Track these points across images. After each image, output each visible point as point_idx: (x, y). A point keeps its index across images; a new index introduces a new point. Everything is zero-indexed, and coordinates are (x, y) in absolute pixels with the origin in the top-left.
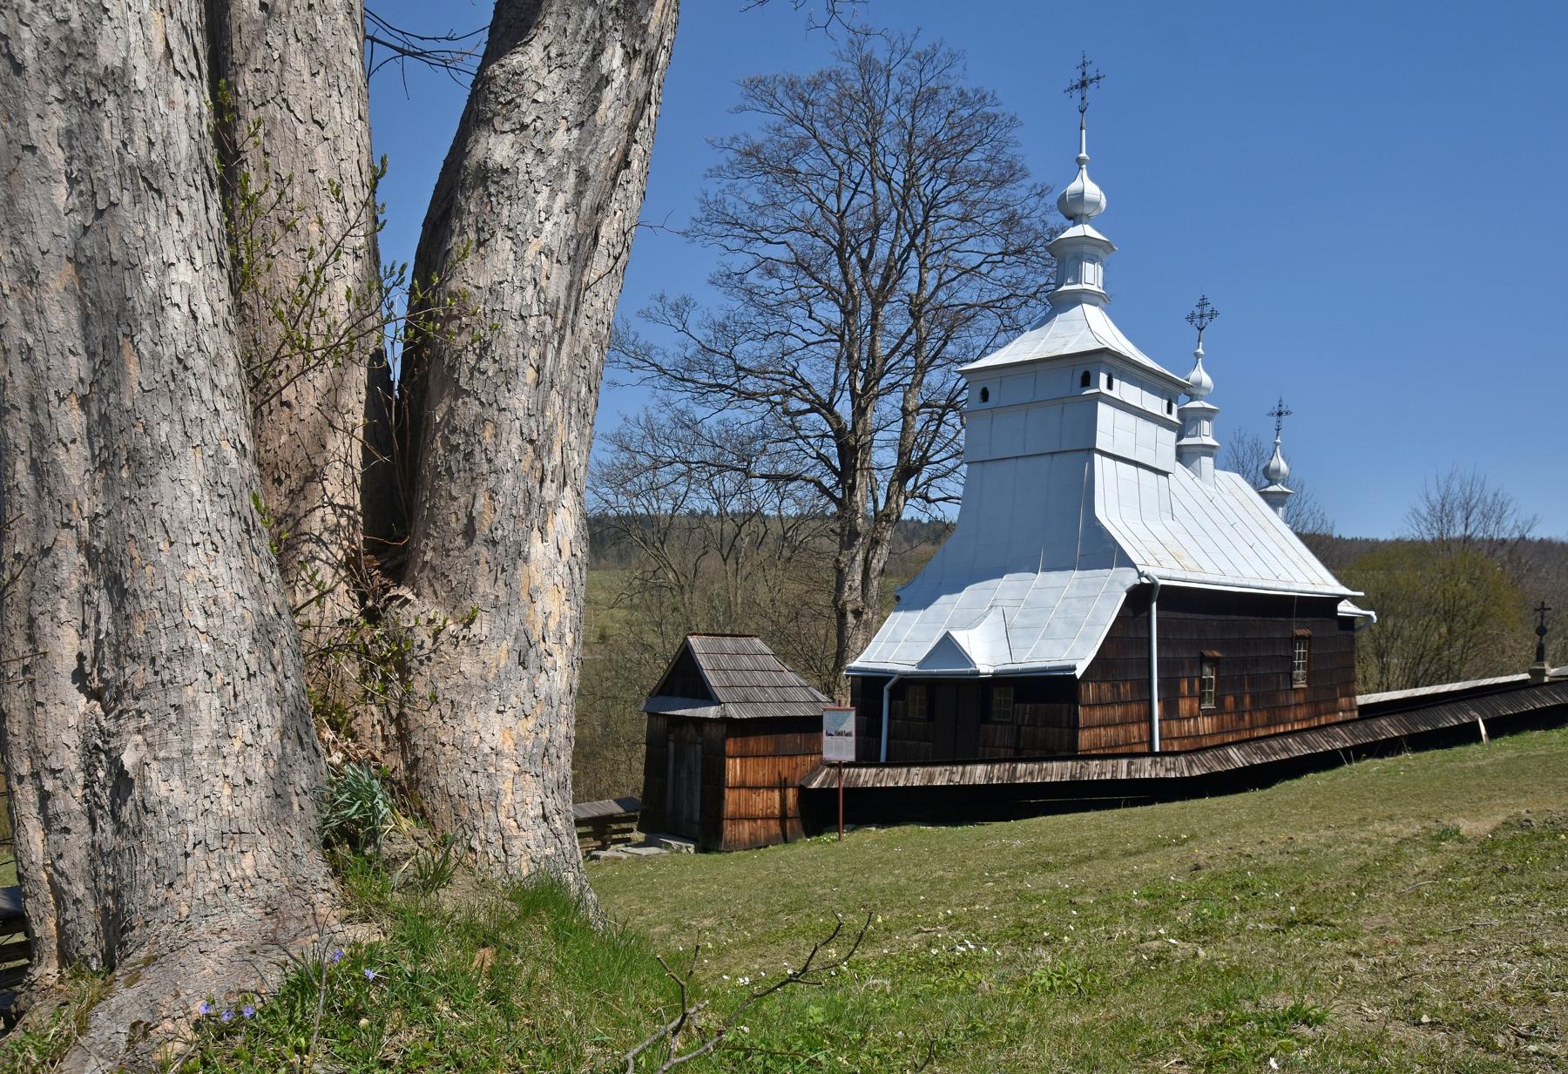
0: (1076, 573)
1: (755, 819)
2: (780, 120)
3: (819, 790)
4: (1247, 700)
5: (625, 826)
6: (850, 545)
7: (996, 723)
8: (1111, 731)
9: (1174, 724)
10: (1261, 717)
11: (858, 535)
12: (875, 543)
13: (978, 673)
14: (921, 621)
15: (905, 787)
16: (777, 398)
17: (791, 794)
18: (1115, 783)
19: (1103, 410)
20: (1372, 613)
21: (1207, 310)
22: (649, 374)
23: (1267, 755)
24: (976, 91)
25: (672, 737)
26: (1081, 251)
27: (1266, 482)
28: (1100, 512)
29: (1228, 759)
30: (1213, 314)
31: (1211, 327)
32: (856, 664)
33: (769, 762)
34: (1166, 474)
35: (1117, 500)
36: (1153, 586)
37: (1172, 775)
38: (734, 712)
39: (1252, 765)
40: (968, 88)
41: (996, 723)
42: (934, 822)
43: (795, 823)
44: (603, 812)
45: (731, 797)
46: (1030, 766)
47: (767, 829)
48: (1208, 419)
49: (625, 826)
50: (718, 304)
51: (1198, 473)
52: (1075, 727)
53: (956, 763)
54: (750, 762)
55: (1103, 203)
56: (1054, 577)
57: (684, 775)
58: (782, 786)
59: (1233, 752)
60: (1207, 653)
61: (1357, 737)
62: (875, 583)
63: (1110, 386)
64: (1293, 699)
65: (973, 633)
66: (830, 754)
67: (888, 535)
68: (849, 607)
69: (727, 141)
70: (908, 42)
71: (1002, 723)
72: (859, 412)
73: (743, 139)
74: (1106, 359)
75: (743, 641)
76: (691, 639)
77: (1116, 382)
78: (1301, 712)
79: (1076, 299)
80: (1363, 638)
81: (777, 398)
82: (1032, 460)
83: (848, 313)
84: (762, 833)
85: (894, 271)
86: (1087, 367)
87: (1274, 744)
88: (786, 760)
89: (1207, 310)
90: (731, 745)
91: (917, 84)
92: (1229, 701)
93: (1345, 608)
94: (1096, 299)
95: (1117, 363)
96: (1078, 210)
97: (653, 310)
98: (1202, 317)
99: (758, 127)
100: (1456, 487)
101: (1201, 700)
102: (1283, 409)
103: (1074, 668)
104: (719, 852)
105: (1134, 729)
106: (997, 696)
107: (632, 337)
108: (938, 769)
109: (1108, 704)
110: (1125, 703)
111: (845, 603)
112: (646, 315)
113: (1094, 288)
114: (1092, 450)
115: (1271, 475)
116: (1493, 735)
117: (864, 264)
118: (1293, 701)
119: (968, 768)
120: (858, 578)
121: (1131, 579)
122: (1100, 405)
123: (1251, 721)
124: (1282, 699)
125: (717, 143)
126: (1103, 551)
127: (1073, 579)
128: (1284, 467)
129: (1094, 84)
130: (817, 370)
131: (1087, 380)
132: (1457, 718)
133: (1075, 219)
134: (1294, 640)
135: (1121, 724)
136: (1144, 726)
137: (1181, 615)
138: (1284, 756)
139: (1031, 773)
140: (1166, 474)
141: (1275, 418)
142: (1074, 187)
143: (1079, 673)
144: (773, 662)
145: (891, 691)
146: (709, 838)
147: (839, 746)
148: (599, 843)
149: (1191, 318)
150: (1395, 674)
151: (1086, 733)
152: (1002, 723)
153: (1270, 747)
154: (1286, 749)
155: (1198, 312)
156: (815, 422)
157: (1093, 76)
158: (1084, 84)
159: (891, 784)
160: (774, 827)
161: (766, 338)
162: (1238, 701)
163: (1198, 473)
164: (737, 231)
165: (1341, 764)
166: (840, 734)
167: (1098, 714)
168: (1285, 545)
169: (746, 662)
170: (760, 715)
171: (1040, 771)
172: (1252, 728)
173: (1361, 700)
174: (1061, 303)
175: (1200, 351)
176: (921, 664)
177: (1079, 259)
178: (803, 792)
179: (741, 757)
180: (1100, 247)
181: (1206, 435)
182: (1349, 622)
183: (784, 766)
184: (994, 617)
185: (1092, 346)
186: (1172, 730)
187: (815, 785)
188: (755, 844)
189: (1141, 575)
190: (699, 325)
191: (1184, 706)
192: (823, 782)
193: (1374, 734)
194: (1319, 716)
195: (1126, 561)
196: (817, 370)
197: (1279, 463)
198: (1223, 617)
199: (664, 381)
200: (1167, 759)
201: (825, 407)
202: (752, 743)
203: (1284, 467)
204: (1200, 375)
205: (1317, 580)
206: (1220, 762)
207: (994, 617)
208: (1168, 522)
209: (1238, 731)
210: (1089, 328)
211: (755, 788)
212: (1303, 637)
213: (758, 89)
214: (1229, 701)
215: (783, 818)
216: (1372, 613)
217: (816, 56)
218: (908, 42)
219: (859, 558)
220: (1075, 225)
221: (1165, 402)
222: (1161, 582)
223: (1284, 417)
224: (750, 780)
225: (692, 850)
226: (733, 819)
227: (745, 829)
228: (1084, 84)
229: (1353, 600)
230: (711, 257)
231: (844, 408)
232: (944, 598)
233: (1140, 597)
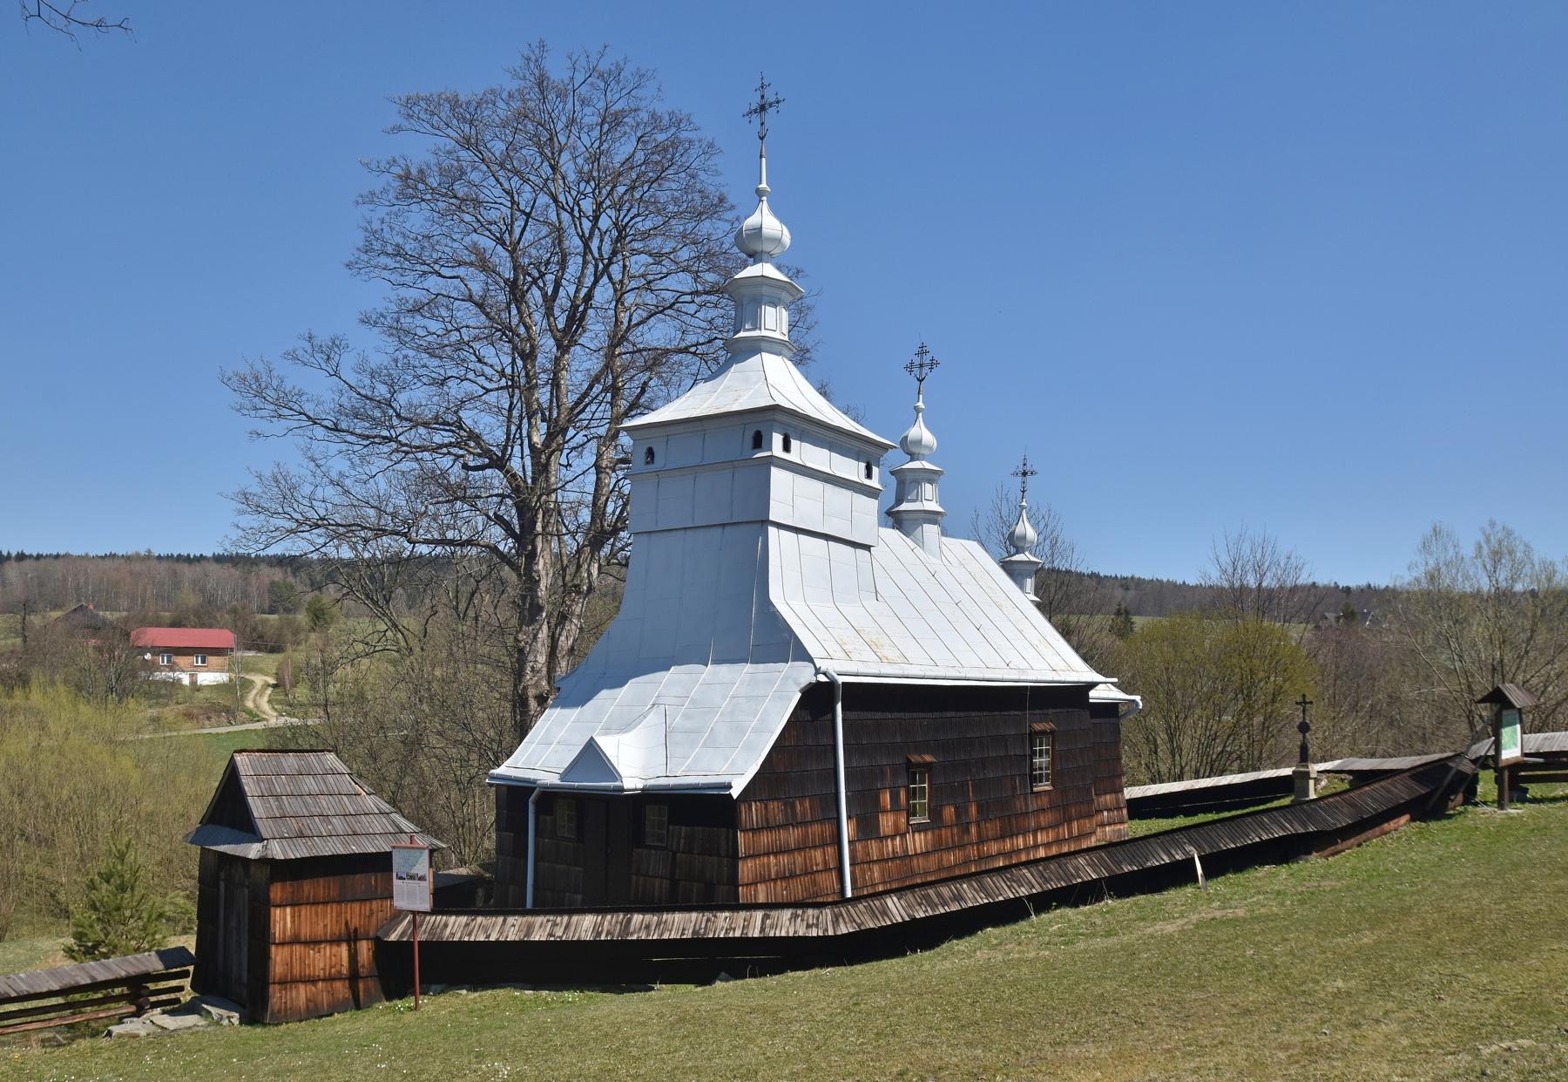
0: (748, 667)
1: (313, 981)
3: (398, 943)
4: (973, 809)
5: (174, 983)
6: (532, 621)
7: (651, 847)
8: (784, 859)
9: (874, 846)
10: (992, 828)
11: (541, 609)
12: (563, 618)
13: (622, 789)
14: (577, 720)
15: (497, 942)
17: (365, 948)
18: (745, 943)
19: (777, 476)
20: (1138, 698)
22: (296, 424)
23: (934, 906)
24: (671, 114)
25: (222, 875)
26: (763, 293)
27: (1013, 550)
28: (775, 595)
29: (885, 912)
30: (933, 364)
31: (931, 377)
32: (502, 770)
33: (332, 910)
34: (867, 548)
35: (796, 582)
36: (832, 684)
37: (814, 933)
38: (277, 851)
39: (914, 920)
40: (661, 109)
41: (651, 847)
42: (536, 985)
43: (371, 983)
44: (142, 969)
45: (279, 956)
46: (648, 917)
47: (332, 993)
48: (931, 482)
49: (174, 983)
50: (376, 348)
51: (921, 543)
52: (734, 857)
53: (561, 912)
54: (305, 911)
55: (787, 238)
56: (724, 669)
57: (233, 924)
58: (352, 938)
59: (892, 903)
60: (915, 758)
61: (1047, 881)
62: (564, 664)
63: (787, 448)
64: (1033, 805)
65: (628, 738)
66: (400, 902)
67: (577, 609)
68: (532, 692)
69: (383, 165)
70: (593, 59)
71: (656, 848)
72: (541, 469)
73: (401, 162)
74: (778, 416)
75: (312, 757)
76: (238, 758)
77: (794, 443)
78: (1044, 819)
79: (755, 347)
80: (1126, 726)
82: (700, 533)
84: (325, 998)
86: (761, 425)
87: (945, 891)
88: (356, 906)
90: (277, 892)
91: (601, 105)
92: (949, 812)
94: (778, 348)
95: (795, 422)
96: (758, 248)
97: (300, 352)
98: (922, 366)
99: (423, 149)
100: (1246, 550)
101: (911, 812)
102: (1028, 469)
103: (729, 787)
104: (264, 1025)
105: (818, 855)
106: (653, 815)
108: (540, 919)
109: (779, 827)
110: (803, 824)
111: (525, 688)
113: (777, 335)
114: (766, 522)
115: (1015, 543)
116: (1208, 875)
117: (549, 301)
118: (1033, 806)
119: (575, 918)
120: (542, 659)
121: (806, 675)
122: (773, 470)
123: (979, 833)
124: (1019, 805)
126: (779, 643)
127: (742, 674)
128: (1031, 534)
131: (759, 441)
132: (1170, 854)
133: (755, 256)
134: (1033, 735)
135: (799, 849)
136: (830, 850)
137: (878, 715)
138: (955, 907)
139: (648, 927)
140: (867, 548)
141: (1020, 478)
142: (752, 221)
143: (735, 793)
144: (346, 783)
145: (537, 803)
146: (255, 1011)
147: (412, 893)
148: (133, 1009)
149: (910, 368)
150: (1189, 755)
151: (750, 863)
152: (656, 848)
153: (939, 895)
154: (958, 898)
155: (917, 361)
157: (772, 99)
158: (763, 108)
159: (482, 938)
160: (341, 989)
162: (961, 812)
163: (921, 543)
165: (1027, 915)
166: (412, 877)
167: (765, 839)
168: (1024, 625)
169: (310, 784)
170: (314, 853)
171: (658, 924)
172: (981, 841)
173: (1132, 792)
174: (741, 351)
175: (920, 404)
176: (563, 776)
177: (758, 302)
178: (381, 947)
179: (292, 905)
180: (783, 289)
181: (929, 499)
182: (1110, 709)
183: (355, 914)
184: (654, 718)
185: (772, 403)
186: (878, 850)
187: (393, 937)
188: (315, 1012)
189: (818, 671)
191: (886, 822)
192: (402, 935)
193: (1069, 876)
194: (1070, 821)
195: (803, 655)
197: (1026, 529)
198: (937, 715)
199: (319, 432)
200: (810, 912)
202: (307, 888)
203: (1031, 534)
204: (921, 432)
206: (874, 916)
207: (654, 718)
208: (871, 603)
209: (962, 846)
210: (774, 380)
211: (314, 942)
212: (1043, 733)
214: (949, 812)
215: (354, 977)
216: (1138, 698)
217: (486, 71)
218: (593, 59)
219: (544, 633)
220: (755, 263)
221: (863, 465)
222: (841, 680)
223: (1028, 477)
224: (305, 932)
225: (236, 1021)
226: (283, 983)
227: (302, 994)
228: (763, 108)
230: (379, 293)
231: (520, 463)
232: (604, 693)
233: (818, 698)
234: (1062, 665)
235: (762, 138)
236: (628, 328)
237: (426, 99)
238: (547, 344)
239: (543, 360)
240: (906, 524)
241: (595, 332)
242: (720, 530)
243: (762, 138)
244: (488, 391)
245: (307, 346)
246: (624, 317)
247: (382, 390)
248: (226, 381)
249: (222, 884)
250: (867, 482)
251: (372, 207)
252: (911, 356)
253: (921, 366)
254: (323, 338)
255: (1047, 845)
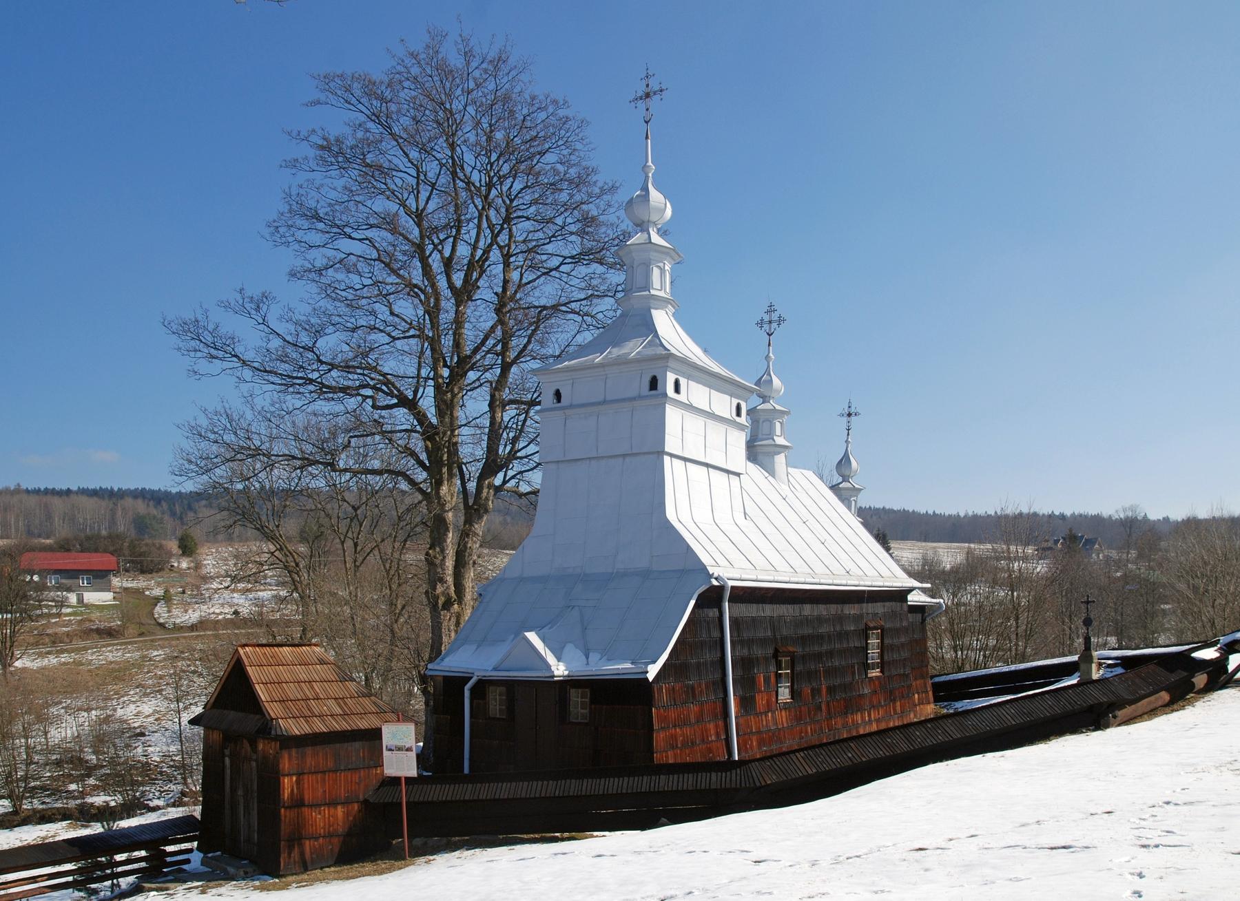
2: (362, 118)
16: (369, 392)
21: (775, 316)
22: (231, 365)
25: (227, 752)
30: (780, 320)
31: (779, 332)
34: (738, 475)
36: (721, 589)
50: (301, 299)
51: (772, 472)
55: (669, 212)
63: (677, 390)
73: (320, 132)
76: (241, 651)
81: (369, 392)
83: (433, 313)
85: (477, 265)
89: (775, 316)
93: (916, 598)
98: (770, 322)
99: (340, 122)
102: (853, 410)
104: (278, 876)
106: (575, 696)
107: (211, 327)
112: (227, 306)
113: (662, 294)
117: (448, 263)
125: (294, 134)
129: (657, 97)
130: (401, 362)
140: (738, 475)
141: (845, 419)
143: (651, 676)
145: (472, 690)
149: (761, 324)
155: (766, 318)
156: (402, 417)
158: (648, 95)
161: (354, 330)
163: (772, 472)
164: (321, 226)
182: (920, 609)
190: (281, 318)
196: (401, 362)
199: (247, 374)
201: (410, 404)
205: (885, 572)
213: (339, 86)
222: (731, 583)
223: (853, 418)
229: (924, 590)
231: (427, 403)
234: (889, 574)
235: (647, 122)
236: (520, 286)
237: (341, 76)
238: (448, 305)
239: (446, 317)
240: (760, 457)
241: (486, 292)
242: (621, 459)
243: (647, 122)
244: (395, 339)
245: (238, 297)
246: (515, 276)
247: (305, 339)
248: (166, 324)
249: (227, 761)
250: (738, 419)
251: (294, 171)
252: (761, 314)
253: (770, 322)
254: (254, 291)
255: (878, 721)
